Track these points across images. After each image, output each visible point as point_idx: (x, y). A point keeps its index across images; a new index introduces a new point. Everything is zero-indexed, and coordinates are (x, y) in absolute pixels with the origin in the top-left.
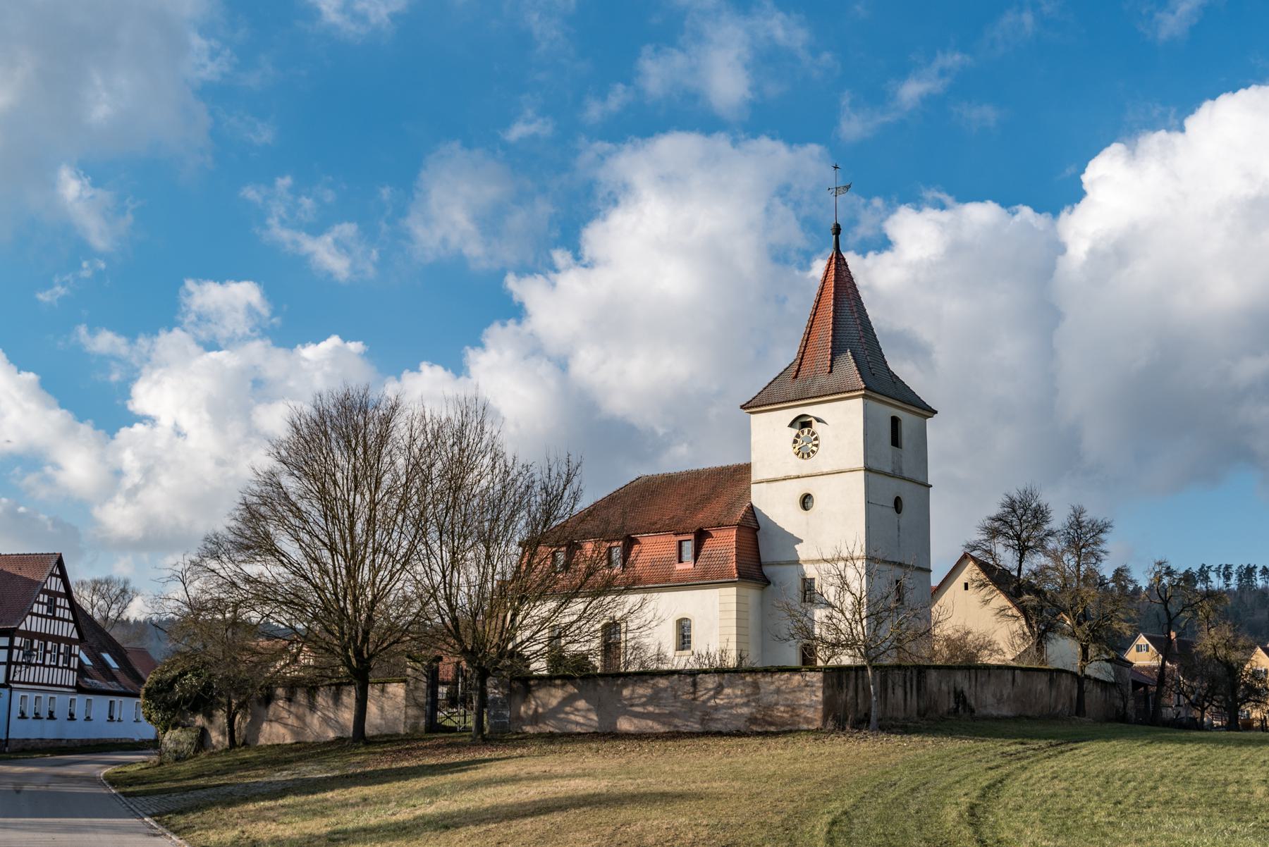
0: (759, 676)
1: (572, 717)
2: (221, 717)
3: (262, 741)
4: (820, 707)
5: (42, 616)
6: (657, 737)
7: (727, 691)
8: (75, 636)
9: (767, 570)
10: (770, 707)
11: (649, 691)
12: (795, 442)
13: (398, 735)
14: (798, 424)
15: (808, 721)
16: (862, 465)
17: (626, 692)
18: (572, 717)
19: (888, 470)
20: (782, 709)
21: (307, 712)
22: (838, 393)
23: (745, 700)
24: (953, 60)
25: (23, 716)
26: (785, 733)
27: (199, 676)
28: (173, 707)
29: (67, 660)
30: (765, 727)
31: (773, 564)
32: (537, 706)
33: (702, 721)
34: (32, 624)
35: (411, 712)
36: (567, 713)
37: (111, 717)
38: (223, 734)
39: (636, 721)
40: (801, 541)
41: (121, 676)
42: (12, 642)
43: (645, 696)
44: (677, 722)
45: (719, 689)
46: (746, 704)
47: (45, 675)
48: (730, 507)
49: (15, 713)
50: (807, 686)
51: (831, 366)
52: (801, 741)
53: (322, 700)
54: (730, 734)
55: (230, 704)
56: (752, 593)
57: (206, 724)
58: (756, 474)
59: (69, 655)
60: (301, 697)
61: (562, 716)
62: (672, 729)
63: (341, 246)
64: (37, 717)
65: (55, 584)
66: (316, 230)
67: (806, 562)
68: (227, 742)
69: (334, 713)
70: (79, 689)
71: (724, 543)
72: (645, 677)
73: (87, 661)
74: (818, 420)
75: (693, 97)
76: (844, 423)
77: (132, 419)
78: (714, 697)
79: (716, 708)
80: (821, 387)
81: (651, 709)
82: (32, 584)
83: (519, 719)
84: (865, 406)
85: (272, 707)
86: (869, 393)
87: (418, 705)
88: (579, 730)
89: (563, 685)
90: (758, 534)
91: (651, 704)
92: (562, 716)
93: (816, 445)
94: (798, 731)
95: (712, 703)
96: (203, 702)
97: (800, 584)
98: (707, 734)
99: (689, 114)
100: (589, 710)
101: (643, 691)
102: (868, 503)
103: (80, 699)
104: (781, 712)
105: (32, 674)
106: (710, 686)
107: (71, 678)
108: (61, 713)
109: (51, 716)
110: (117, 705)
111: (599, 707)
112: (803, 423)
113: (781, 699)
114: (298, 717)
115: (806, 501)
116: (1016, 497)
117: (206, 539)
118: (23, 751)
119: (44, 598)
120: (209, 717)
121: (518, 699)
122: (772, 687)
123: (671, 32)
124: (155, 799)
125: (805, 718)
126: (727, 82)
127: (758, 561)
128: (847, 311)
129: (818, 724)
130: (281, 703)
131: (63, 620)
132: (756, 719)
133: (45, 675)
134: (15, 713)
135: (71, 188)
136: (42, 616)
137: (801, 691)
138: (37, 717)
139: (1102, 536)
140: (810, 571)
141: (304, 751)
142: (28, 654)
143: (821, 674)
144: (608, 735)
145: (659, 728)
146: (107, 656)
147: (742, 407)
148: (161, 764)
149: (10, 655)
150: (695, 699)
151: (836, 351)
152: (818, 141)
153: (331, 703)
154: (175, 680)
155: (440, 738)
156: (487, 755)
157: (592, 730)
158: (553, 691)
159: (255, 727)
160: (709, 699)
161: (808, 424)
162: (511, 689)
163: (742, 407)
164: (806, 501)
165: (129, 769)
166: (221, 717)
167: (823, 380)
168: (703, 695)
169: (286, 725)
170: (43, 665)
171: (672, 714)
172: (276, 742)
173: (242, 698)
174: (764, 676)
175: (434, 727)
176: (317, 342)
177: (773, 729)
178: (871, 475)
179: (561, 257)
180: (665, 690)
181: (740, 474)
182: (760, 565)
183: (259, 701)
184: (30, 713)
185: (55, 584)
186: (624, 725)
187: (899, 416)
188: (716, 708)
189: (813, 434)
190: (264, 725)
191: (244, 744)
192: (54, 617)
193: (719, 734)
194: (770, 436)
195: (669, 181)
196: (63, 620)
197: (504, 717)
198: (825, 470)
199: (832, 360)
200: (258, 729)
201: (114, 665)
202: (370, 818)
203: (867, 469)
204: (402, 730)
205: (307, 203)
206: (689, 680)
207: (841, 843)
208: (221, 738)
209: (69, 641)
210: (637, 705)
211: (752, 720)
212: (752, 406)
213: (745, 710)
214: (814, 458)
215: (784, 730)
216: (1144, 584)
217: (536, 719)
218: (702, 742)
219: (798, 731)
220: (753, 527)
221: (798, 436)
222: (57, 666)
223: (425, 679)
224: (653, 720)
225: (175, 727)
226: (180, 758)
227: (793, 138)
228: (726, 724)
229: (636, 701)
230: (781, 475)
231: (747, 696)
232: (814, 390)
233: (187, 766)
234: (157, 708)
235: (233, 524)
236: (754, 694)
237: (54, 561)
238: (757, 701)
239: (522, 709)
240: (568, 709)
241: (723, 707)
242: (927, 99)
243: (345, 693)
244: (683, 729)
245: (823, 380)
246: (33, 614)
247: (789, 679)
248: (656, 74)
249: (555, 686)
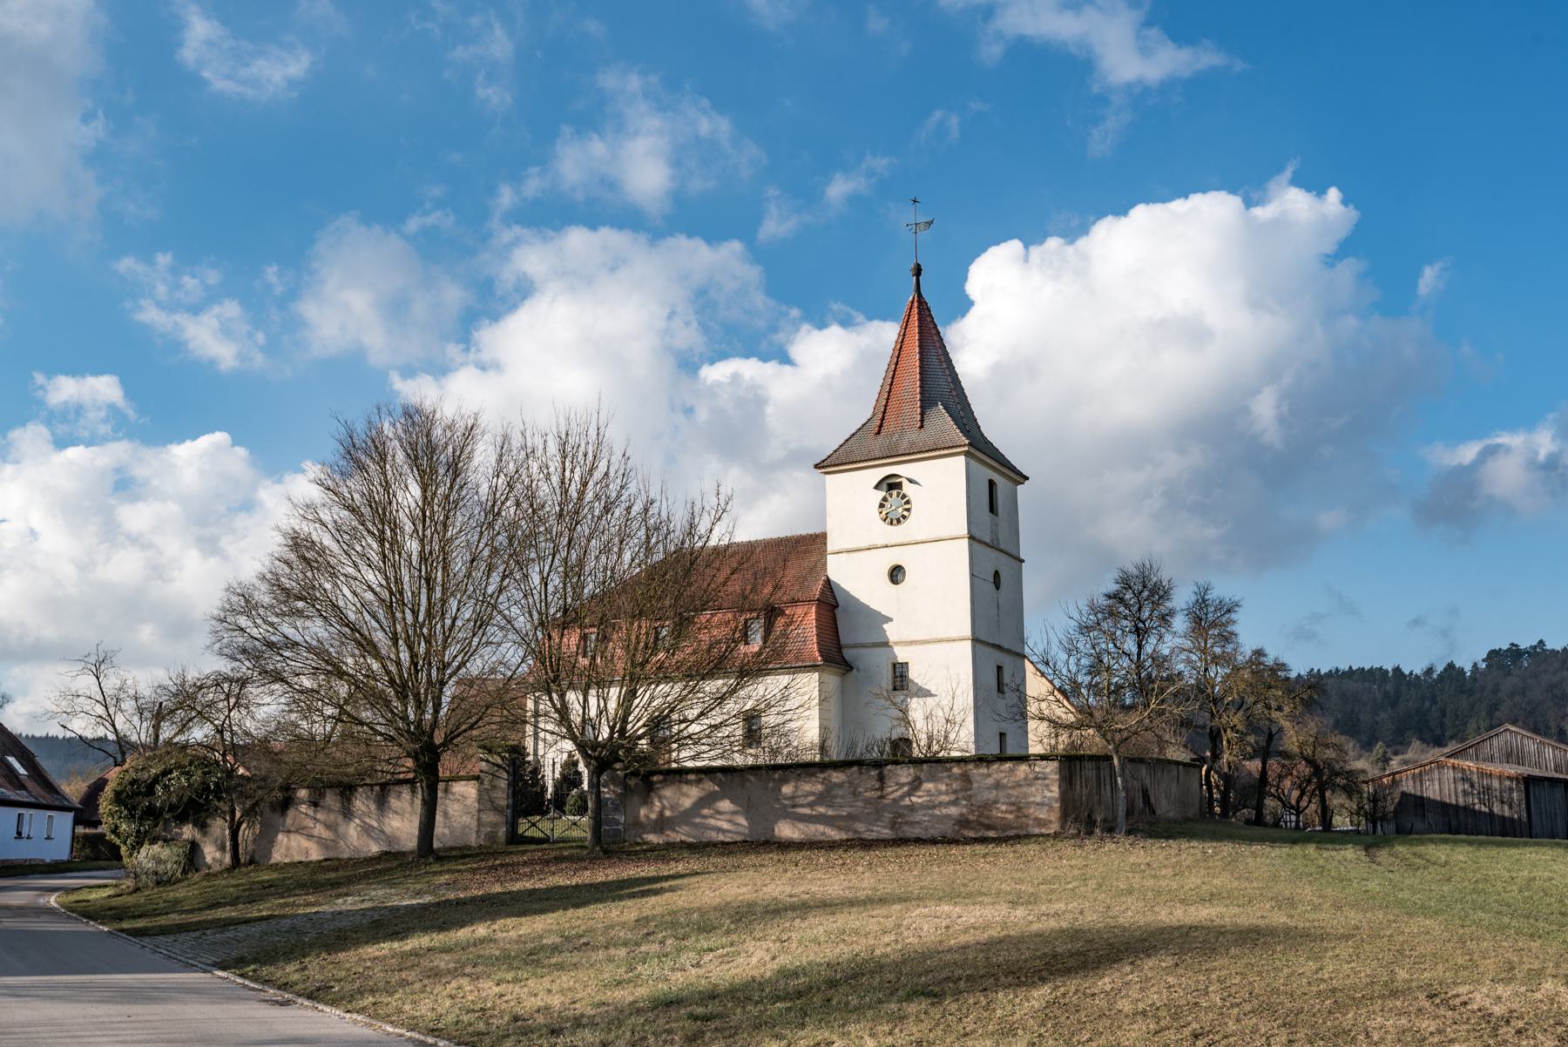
0: (971, 766)
1: (712, 822)
3: (277, 856)
4: (1057, 805)
6: (832, 846)
7: (928, 786)
10: (987, 805)
11: (819, 787)
12: (882, 506)
14: (885, 486)
15: (1040, 823)
18: (712, 822)
19: (988, 540)
20: (1004, 808)
21: (340, 819)
23: (952, 797)
24: (881, 163)
27: (189, 774)
30: (981, 830)
31: (856, 646)
32: (663, 808)
36: (705, 817)
37: (19, 834)
38: (222, 848)
39: (801, 826)
40: (889, 620)
41: (30, 784)
43: (813, 794)
44: (860, 827)
45: (916, 784)
46: (954, 803)
48: (803, 581)
50: (1037, 778)
51: (922, 421)
52: (1032, 849)
54: (934, 842)
55: (233, 812)
56: (833, 680)
57: (198, 836)
58: (832, 545)
60: (331, 799)
61: (698, 820)
62: (851, 835)
63: (226, 331)
66: (195, 310)
67: (897, 643)
68: (228, 859)
69: (378, 821)
71: (806, 625)
72: (812, 770)
74: (911, 481)
75: (611, 184)
76: (941, 485)
78: (909, 794)
79: (912, 808)
81: (822, 810)
83: (637, 824)
84: (967, 464)
85: (291, 813)
87: (497, 809)
88: (721, 838)
89: (699, 781)
90: (838, 612)
91: (821, 804)
92: (698, 820)
95: (907, 801)
96: (195, 809)
97: (890, 668)
99: (603, 208)
100: (734, 813)
101: (812, 787)
102: (972, 575)
104: (1002, 811)
106: (904, 780)
111: (748, 808)
112: (891, 485)
114: (328, 827)
116: (1133, 570)
117: (227, 590)
120: (203, 827)
121: (636, 799)
122: (990, 781)
123: (597, 117)
124: (211, 936)
125: (1037, 819)
126: (646, 172)
127: (847, 645)
128: (934, 359)
130: (303, 808)
132: (968, 821)
137: (1030, 785)
139: (1233, 616)
140: (902, 654)
141: (336, 873)
143: (1056, 764)
145: (835, 834)
147: (817, 466)
148: (137, 890)
151: (927, 403)
152: (739, 238)
153: (373, 807)
154: (156, 780)
155: (533, 853)
156: (681, 868)
157: (739, 838)
158: (685, 788)
159: (266, 839)
160: (902, 797)
161: (899, 486)
162: (626, 787)
163: (817, 466)
164: (896, 574)
165: (94, 896)
166: (219, 827)
167: (913, 436)
168: (893, 791)
169: (310, 836)
171: (850, 817)
172: (297, 858)
173: (249, 803)
174: (977, 767)
175: (515, 838)
176: (194, 438)
177: (992, 834)
179: (453, 351)
180: (841, 785)
181: (811, 545)
182: (840, 647)
183: (273, 808)
189: (904, 496)
190: (280, 836)
191: (251, 862)
193: (919, 841)
195: (578, 279)
197: (617, 823)
198: (919, 539)
199: (922, 414)
201: (22, 771)
202: (753, 958)
203: (971, 538)
204: (473, 840)
205: (189, 282)
206: (873, 773)
208: (218, 855)
210: (803, 806)
211: (963, 822)
212: (830, 464)
213: (953, 811)
215: (1012, 835)
217: (661, 824)
220: (831, 602)
221: (885, 499)
223: (505, 775)
225: (153, 841)
226: (162, 881)
227: (714, 237)
228: (926, 829)
229: (802, 801)
230: (866, 545)
231: (955, 792)
233: (180, 892)
234: (131, 817)
236: (965, 789)
238: (969, 798)
239: (643, 812)
240: (705, 811)
241: (922, 806)
242: (853, 200)
243: (393, 795)
244: (867, 836)
247: (1011, 770)
248: (575, 162)
249: (687, 782)
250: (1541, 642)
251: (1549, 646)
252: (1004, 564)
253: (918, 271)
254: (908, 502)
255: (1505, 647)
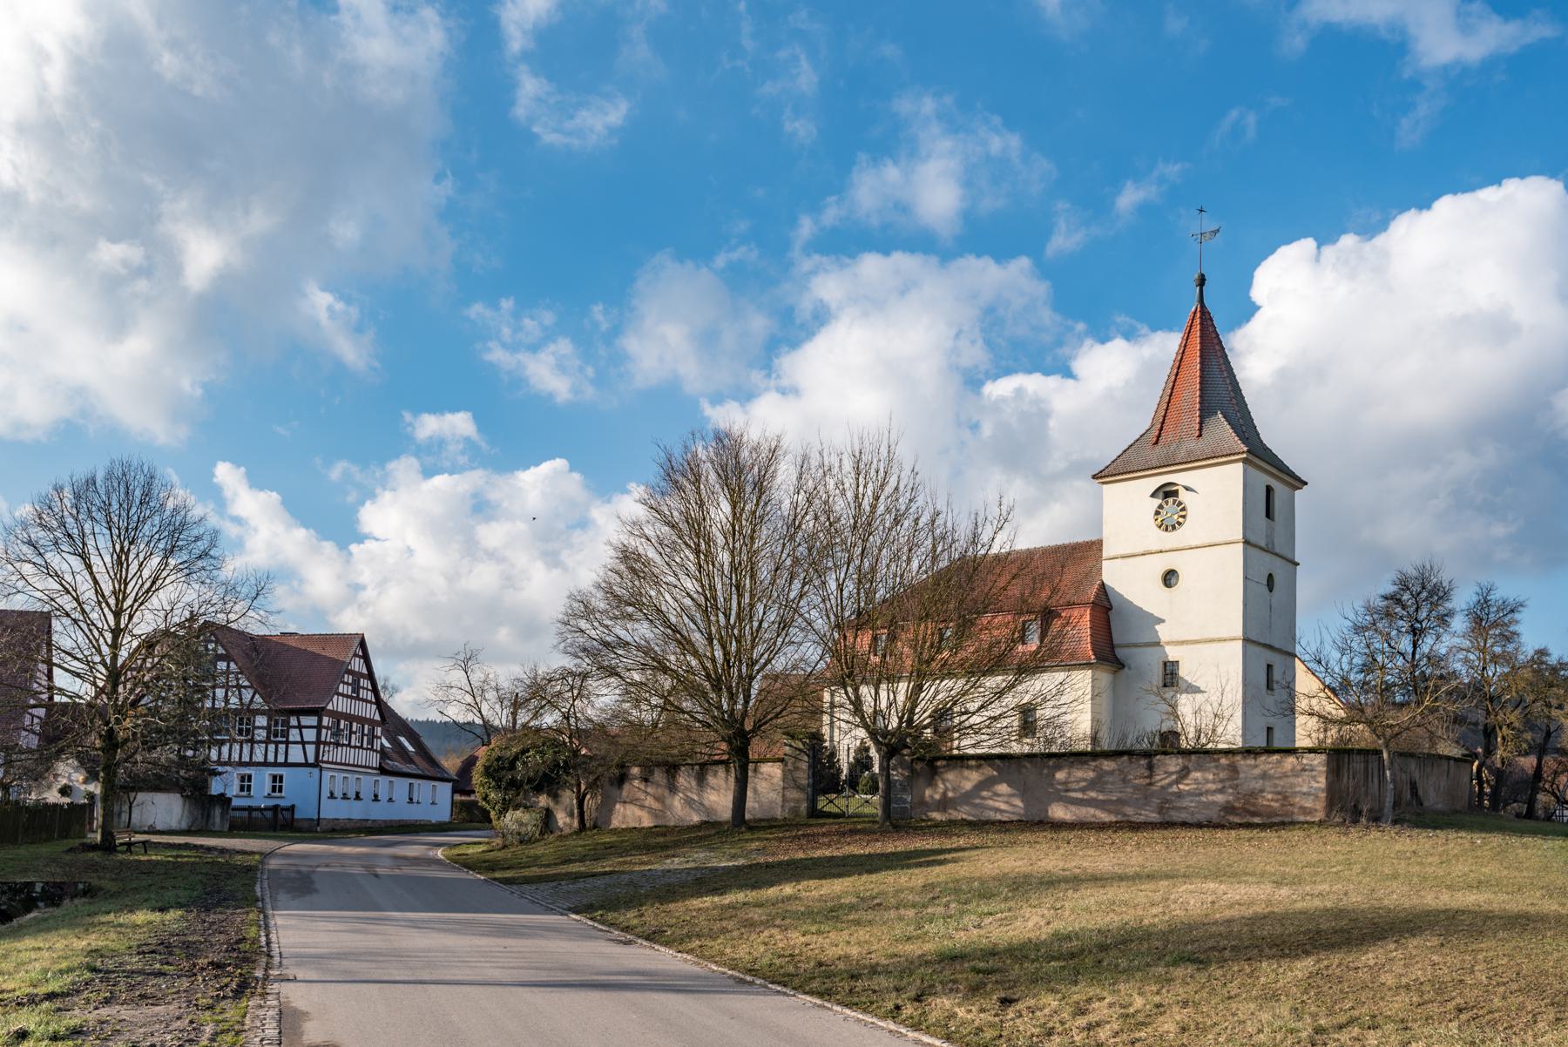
0: (1238, 757)
1: (991, 803)
2: (568, 797)
3: (616, 823)
5: (347, 696)
6: (1102, 827)
8: (377, 717)
9: (1120, 653)
10: (1253, 794)
11: (1091, 774)
12: (1157, 513)
13: (776, 820)
14: (1161, 494)
15: (1304, 811)
16: (1240, 536)
17: (1060, 776)
18: (991, 803)
19: (1263, 544)
21: (667, 793)
22: (1213, 457)
23: (1220, 786)
24: (1173, 170)
25: (332, 796)
26: (1283, 825)
28: (514, 784)
29: (371, 742)
33: (1160, 810)
34: (339, 704)
35: (793, 794)
38: (571, 815)
39: (1073, 808)
41: (417, 759)
42: (320, 721)
45: (1184, 773)
46: (1221, 791)
47: (351, 756)
48: (1078, 586)
49: (325, 793)
50: (1304, 770)
51: (1201, 430)
52: (1296, 835)
53: (684, 780)
54: (1200, 826)
55: (579, 785)
56: (1105, 677)
57: (551, 804)
58: (1107, 552)
59: (373, 737)
60: (659, 776)
62: (1120, 818)
63: (561, 368)
64: (345, 797)
65: (358, 665)
67: (1168, 643)
68: (576, 824)
70: (383, 771)
71: (1081, 627)
73: (387, 744)
74: (1187, 489)
76: (1217, 493)
77: (361, 538)
78: (1177, 782)
80: (1189, 452)
81: (1093, 794)
82: (335, 663)
83: (923, 802)
84: (1245, 471)
85: (626, 787)
86: (1251, 457)
87: (799, 788)
88: (999, 817)
94: (1293, 823)
95: (1174, 789)
96: (548, 782)
97: (1161, 665)
98: (1168, 825)
101: (1084, 774)
102: (1245, 578)
103: (384, 780)
104: (1268, 799)
105: (339, 754)
106: (1172, 769)
107: (374, 760)
108: (366, 794)
109: (358, 797)
110: (416, 787)
111: (1024, 791)
113: (1268, 785)
114: (657, 799)
115: (1169, 578)
118: (333, 830)
119: (348, 678)
120: (555, 797)
121: (921, 781)
122: (1257, 772)
123: (893, 143)
127: (1114, 640)
129: (1320, 816)
130: (636, 783)
131: (366, 701)
133: (351, 756)
134: (325, 793)
135: (320, 301)
136: (347, 696)
138: (345, 797)
139: (1517, 616)
140: (1172, 653)
141: (664, 838)
142: (337, 733)
143: (1324, 757)
144: (1037, 823)
145: (1105, 817)
146: (402, 739)
147: (1094, 477)
148: (505, 847)
149: (319, 734)
150: (1150, 784)
151: (1206, 412)
153: (694, 783)
154: (516, 758)
158: (966, 773)
159: (607, 807)
160: (1170, 785)
161: (1175, 493)
162: (913, 771)
163: (1094, 477)
166: (568, 797)
167: (1192, 444)
168: (1161, 779)
169: (642, 807)
170: (349, 745)
171: (1120, 801)
172: (632, 825)
173: (591, 778)
175: (815, 813)
176: (537, 465)
177: (1257, 820)
178: (1252, 550)
180: (1112, 773)
181: (1089, 551)
182: (1113, 647)
184: (338, 794)
185: (358, 665)
186: (1058, 812)
187: (1273, 481)
188: (1180, 795)
190: (618, 806)
191: (595, 827)
192: (358, 698)
193: (1185, 825)
194: (1126, 512)
195: (872, 304)
196: (366, 701)
197: (905, 801)
198: (1193, 544)
199: (1201, 423)
200: (611, 811)
201: (411, 748)
203: (1246, 542)
204: (779, 813)
205: (528, 323)
206: (1143, 762)
209: (372, 722)
211: (1229, 809)
212: (1105, 475)
213: (1219, 798)
214: (1180, 531)
217: (944, 804)
218: (1119, 837)
219: (1293, 823)
220: (1105, 606)
221: (1161, 507)
222: (361, 747)
224: (1096, 807)
225: (516, 808)
226: (525, 840)
227: (1002, 255)
229: (1074, 786)
231: (1222, 781)
232: (1181, 456)
233: (538, 850)
237: (357, 641)
240: (985, 793)
241: (1190, 793)
242: (1144, 209)
245: (1192, 444)
246: (339, 694)
247: (1279, 762)
248: (871, 188)
249: (968, 767)
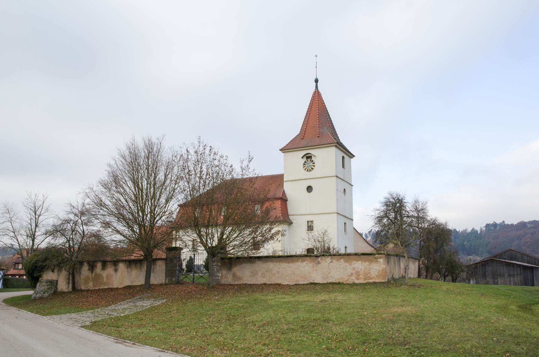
12: (304, 164)
14: (305, 158)
58: (285, 179)
68: (70, 289)
86: (338, 145)
93: (312, 169)
147: (280, 150)
161: (310, 157)
163: (280, 150)
164: (309, 189)
189: (312, 161)
197: (218, 276)
207: (1, 230)
216: (142, 253)
221: (305, 162)
235: (113, 163)
250: (504, 221)
251: (506, 223)
252: (347, 186)
253: (317, 81)
254: (314, 163)
255: (491, 223)
